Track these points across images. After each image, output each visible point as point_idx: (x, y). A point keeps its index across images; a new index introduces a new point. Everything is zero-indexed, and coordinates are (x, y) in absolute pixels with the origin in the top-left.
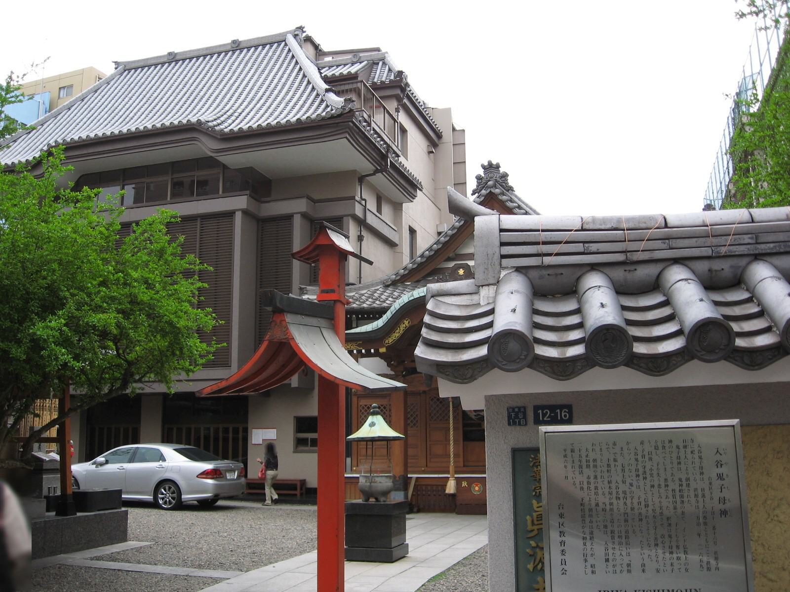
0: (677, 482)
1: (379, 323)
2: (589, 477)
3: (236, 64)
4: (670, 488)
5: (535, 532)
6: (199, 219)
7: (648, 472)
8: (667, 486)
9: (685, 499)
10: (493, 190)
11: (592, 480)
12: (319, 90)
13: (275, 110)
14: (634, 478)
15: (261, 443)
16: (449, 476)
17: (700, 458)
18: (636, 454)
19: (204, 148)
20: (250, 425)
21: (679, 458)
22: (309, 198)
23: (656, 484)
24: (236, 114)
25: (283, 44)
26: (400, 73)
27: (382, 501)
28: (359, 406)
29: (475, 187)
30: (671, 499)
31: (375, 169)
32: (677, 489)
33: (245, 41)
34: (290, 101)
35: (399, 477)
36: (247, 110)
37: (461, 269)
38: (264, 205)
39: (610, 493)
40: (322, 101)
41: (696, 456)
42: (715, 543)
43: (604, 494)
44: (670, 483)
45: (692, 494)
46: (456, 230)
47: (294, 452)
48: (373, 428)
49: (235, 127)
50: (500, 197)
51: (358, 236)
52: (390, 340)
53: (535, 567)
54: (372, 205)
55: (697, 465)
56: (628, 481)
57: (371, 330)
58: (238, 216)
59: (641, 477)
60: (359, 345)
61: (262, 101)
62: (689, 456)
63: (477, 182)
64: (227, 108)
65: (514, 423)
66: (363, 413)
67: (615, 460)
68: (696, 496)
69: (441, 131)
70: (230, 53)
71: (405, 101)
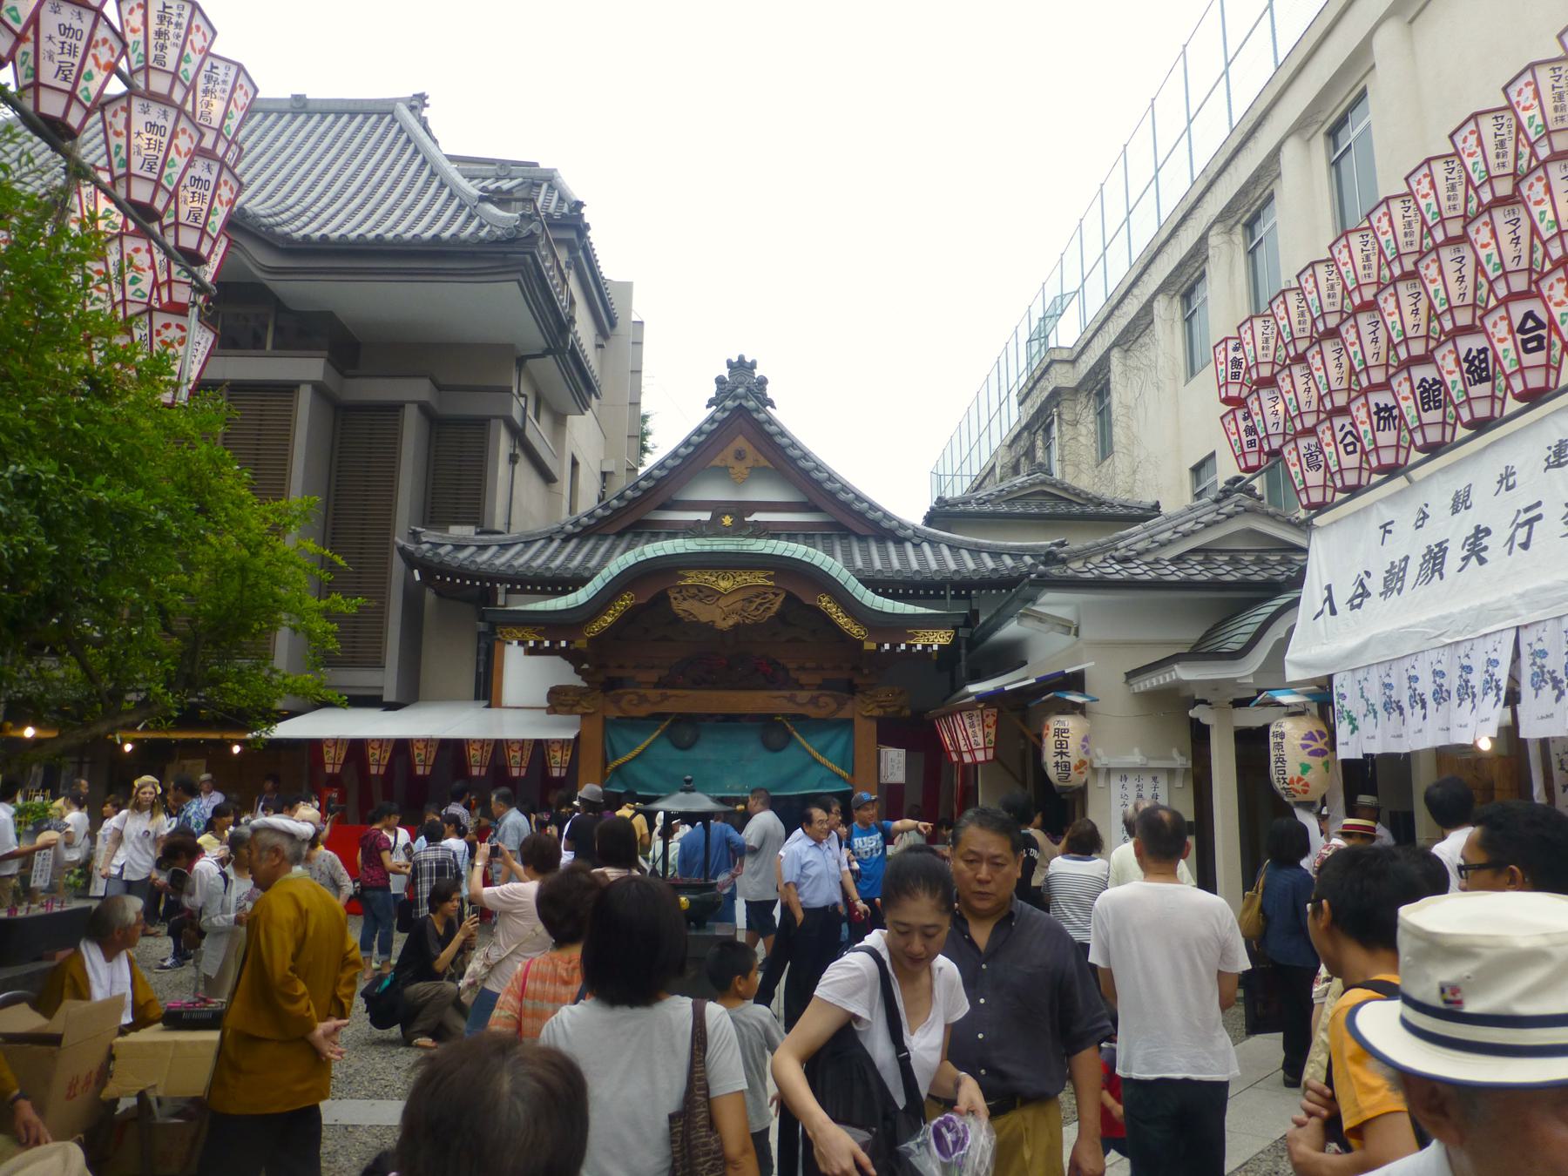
1: (581, 596)
3: (302, 134)
10: (744, 403)
19: (246, 261)
24: (310, 214)
25: (388, 118)
26: (580, 205)
33: (315, 101)
36: (331, 211)
38: (349, 381)
40: (471, 217)
49: (313, 230)
50: (755, 415)
54: (530, 413)
58: (305, 394)
60: (539, 633)
61: (357, 201)
64: (290, 202)
70: (287, 117)
71: (581, 253)
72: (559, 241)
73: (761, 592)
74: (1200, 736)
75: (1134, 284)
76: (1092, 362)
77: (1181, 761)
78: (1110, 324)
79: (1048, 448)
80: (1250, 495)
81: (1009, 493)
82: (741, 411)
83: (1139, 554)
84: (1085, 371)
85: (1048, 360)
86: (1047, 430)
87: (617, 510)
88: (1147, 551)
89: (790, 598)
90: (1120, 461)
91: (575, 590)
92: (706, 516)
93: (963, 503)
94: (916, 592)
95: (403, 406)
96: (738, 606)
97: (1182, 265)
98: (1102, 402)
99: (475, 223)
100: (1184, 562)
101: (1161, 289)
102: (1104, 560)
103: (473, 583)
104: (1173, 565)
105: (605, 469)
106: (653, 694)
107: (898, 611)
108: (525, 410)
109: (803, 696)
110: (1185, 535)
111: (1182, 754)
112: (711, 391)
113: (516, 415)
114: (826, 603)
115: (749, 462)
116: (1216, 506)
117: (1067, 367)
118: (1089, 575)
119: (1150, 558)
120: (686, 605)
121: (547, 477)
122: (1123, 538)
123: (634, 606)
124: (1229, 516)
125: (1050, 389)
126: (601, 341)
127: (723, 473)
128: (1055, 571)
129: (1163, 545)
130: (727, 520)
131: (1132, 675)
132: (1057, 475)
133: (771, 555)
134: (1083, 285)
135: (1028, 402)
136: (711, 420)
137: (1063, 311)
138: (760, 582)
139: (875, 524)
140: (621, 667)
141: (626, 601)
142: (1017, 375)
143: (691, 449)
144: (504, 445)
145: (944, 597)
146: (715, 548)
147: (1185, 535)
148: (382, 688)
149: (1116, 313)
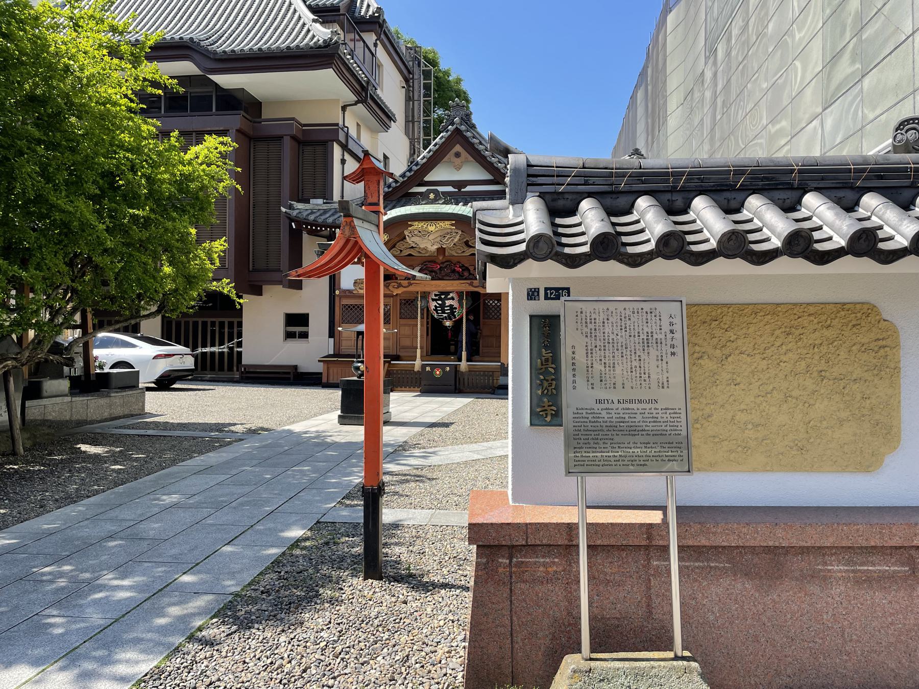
0: (645, 334)
2: (591, 329)
4: (641, 338)
5: (544, 370)
6: (194, 133)
7: (628, 328)
8: (639, 336)
9: (650, 345)
11: (593, 331)
12: (306, 19)
14: (619, 330)
17: (660, 319)
18: (621, 316)
21: (647, 319)
23: (632, 335)
30: (641, 344)
32: (645, 338)
39: (604, 340)
41: (658, 318)
42: (667, 372)
43: (600, 340)
44: (641, 334)
45: (654, 341)
53: (543, 392)
55: (658, 324)
56: (615, 332)
59: (623, 331)
62: (653, 318)
65: (531, 299)
67: (608, 319)
68: (657, 343)
87: (395, 189)
138: (448, 226)
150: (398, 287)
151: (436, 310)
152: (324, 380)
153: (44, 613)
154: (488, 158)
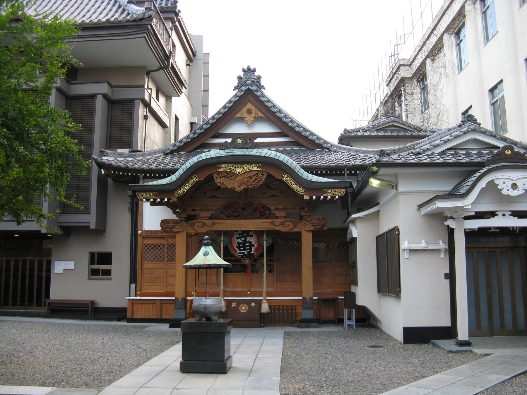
1: (173, 178)
10: (250, 87)
13: (86, 13)
15: (62, 272)
16: (262, 298)
20: (53, 258)
22: (109, 84)
27: (214, 320)
28: (143, 244)
29: (236, 85)
31: (160, 66)
34: (98, 8)
35: (181, 299)
37: (239, 139)
38: (71, 86)
40: (124, 10)
46: (221, 115)
47: (88, 280)
48: (207, 257)
50: (256, 93)
51: (145, 116)
52: (180, 193)
54: (154, 95)
57: (176, 179)
60: (155, 195)
63: (238, 81)
66: (160, 246)
69: (196, 51)
71: (177, 23)
72: (166, 19)
73: (255, 174)
74: (451, 232)
75: (434, 29)
76: (418, 65)
77: (442, 245)
78: (425, 48)
79: (400, 105)
80: (474, 123)
81: (377, 126)
82: (249, 91)
83: (424, 151)
84: (415, 69)
85: (398, 64)
86: (400, 97)
88: (428, 149)
89: (269, 176)
90: (432, 111)
91: (169, 176)
92: (229, 140)
93: (357, 132)
94: (331, 172)
95: (96, 96)
96: (246, 180)
97: (454, 20)
98: (424, 84)
99: (126, 13)
100: (445, 154)
101: (446, 30)
102: (408, 154)
103: (128, 174)
104: (439, 155)
105: (192, 122)
106: (209, 222)
107: (328, 181)
108: (150, 95)
109: (277, 221)
110: (445, 142)
111: (444, 242)
112: (236, 83)
113: (147, 97)
114: (286, 178)
115: (253, 115)
116: (459, 128)
117: (407, 67)
118: (400, 161)
119: (429, 153)
120: (222, 180)
121: (163, 125)
122: (418, 144)
123: (197, 182)
124: (465, 133)
125: (400, 78)
126: (189, 63)
127: (242, 120)
128: (385, 159)
129: (435, 147)
130: (239, 141)
131: (421, 206)
132: (404, 118)
133: (259, 156)
134: (413, 30)
135: (391, 84)
136: (236, 96)
137: (405, 42)
138: (255, 169)
139: (313, 142)
140: (194, 210)
141: (194, 179)
142: (385, 74)
143: (226, 110)
144: (142, 111)
145: (344, 175)
146: (234, 154)
147: (445, 142)
148: (89, 222)
149: (427, 42)
150: (203, 226)
151: (238, 247)
152: (129, 315)
153: (432, 391)
154: (277, 114)
